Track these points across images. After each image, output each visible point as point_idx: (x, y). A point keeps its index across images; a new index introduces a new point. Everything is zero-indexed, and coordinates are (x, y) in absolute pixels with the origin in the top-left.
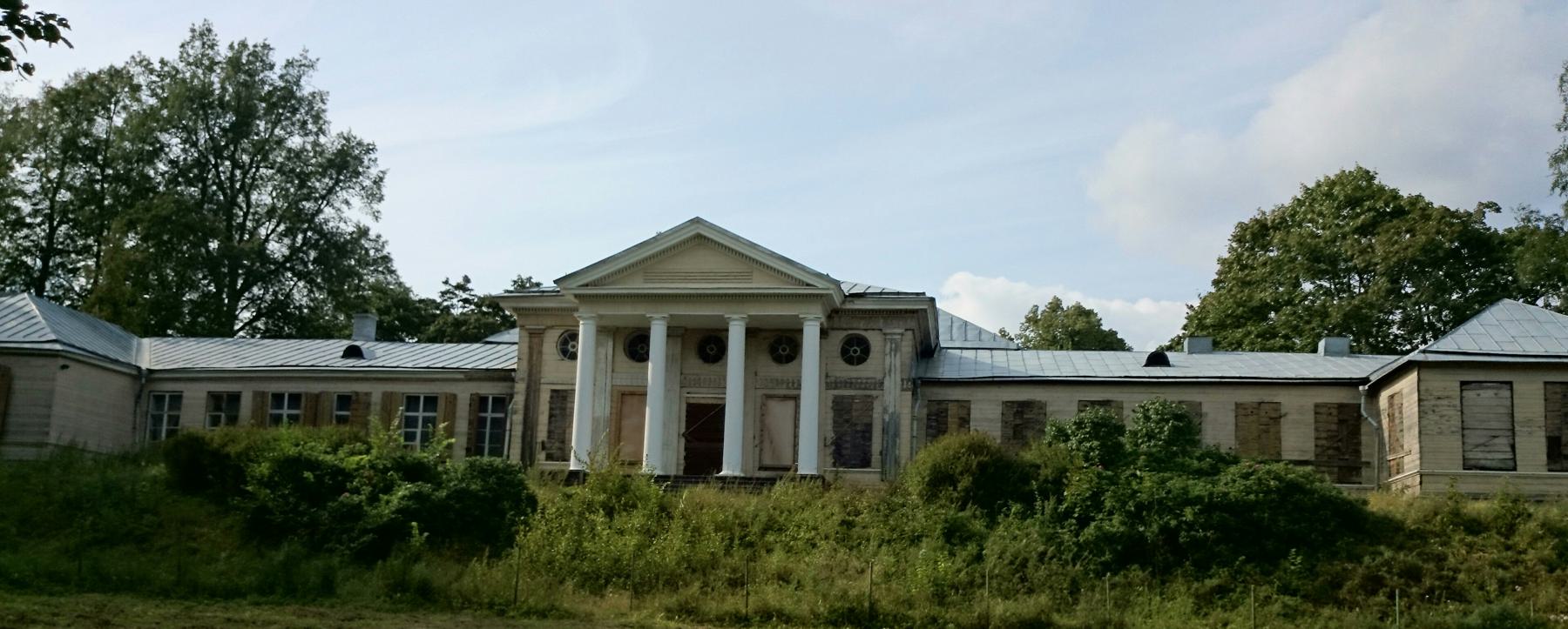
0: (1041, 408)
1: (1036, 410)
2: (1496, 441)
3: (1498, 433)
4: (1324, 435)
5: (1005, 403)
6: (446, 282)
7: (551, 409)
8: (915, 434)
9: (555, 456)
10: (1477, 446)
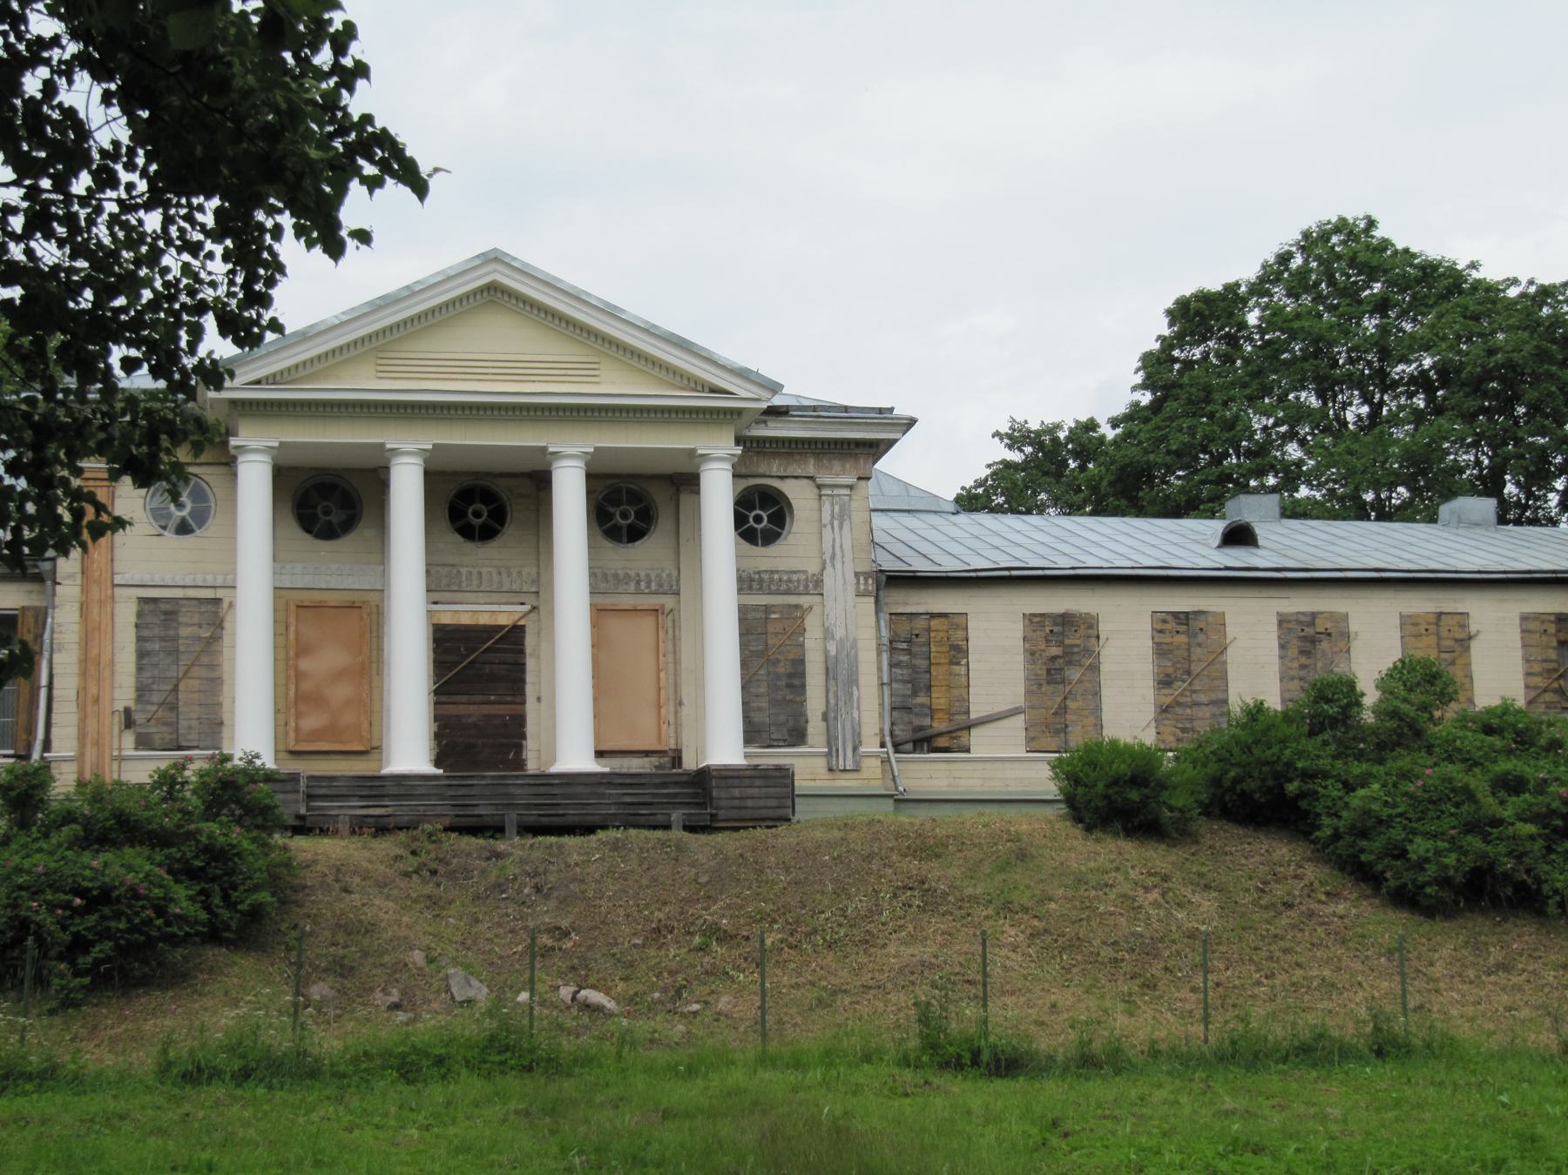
0: (1090, 627)
1: (1082, 630)
4: (1537, 668)
5: (1524, 618)
7: (140, 639)
8: (886, 680)
9: (157, 739)
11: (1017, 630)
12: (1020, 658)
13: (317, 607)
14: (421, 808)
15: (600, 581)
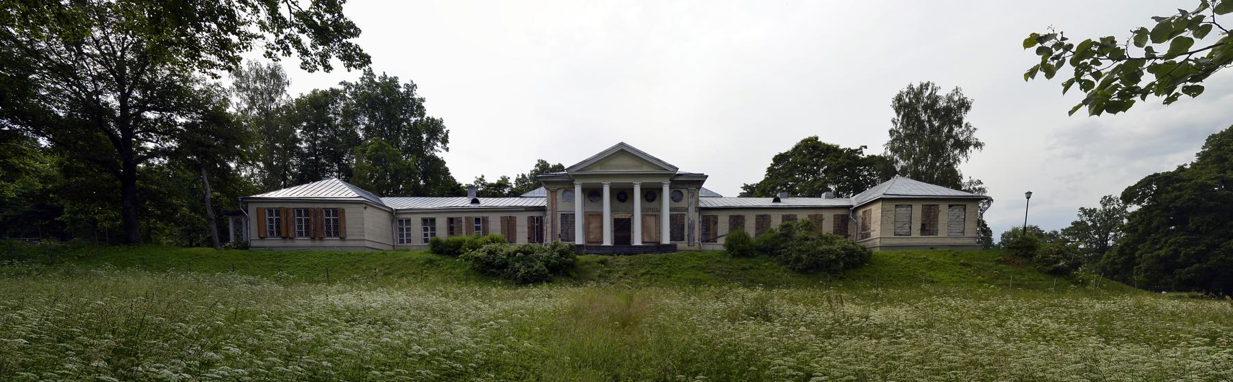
5: (835, 215)
11: (728, 218)
12: (728, 224)
13: (592, 215)
14: (292, 227)
15: (643, 209)
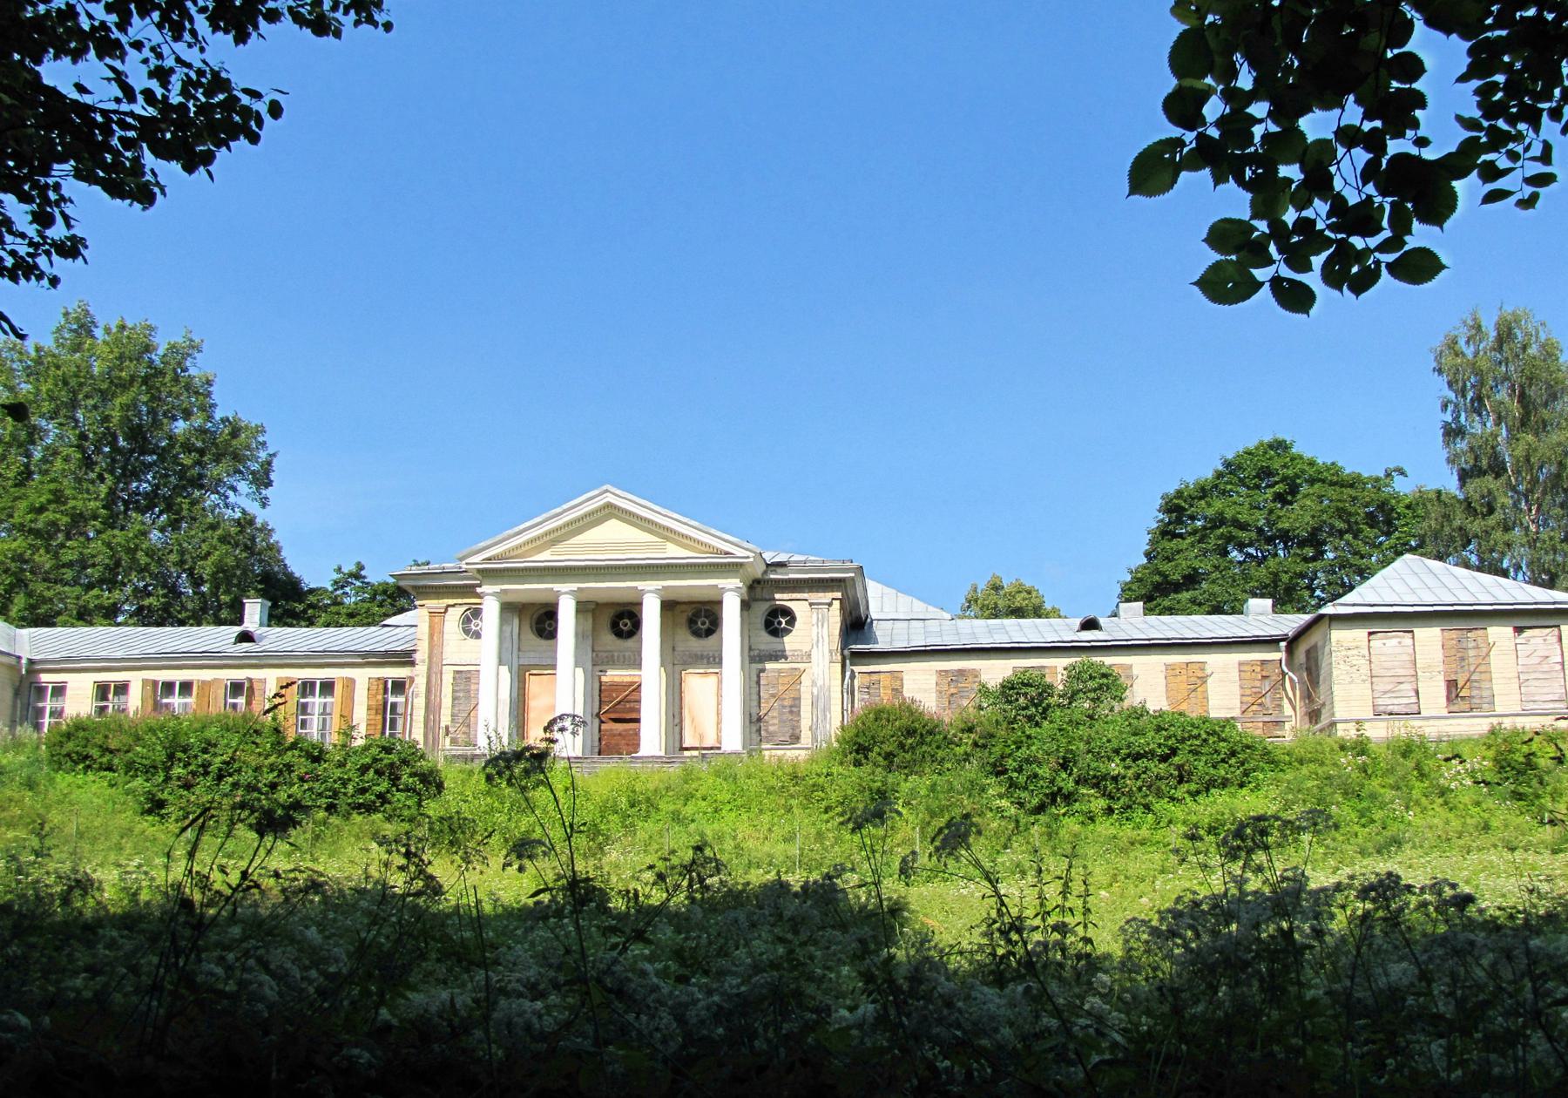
1: (970, 679)
2: (1402, 686)
3: (1402, 680)
4: (1248, 692)
6: (339, 570)
7: (454, 691)
10: (1385, 693)
11: (934, 679)
